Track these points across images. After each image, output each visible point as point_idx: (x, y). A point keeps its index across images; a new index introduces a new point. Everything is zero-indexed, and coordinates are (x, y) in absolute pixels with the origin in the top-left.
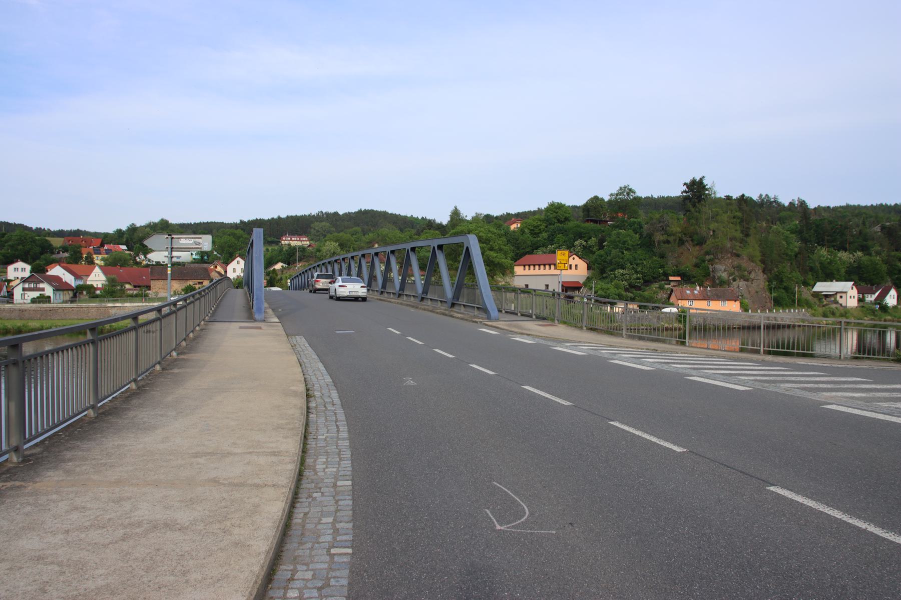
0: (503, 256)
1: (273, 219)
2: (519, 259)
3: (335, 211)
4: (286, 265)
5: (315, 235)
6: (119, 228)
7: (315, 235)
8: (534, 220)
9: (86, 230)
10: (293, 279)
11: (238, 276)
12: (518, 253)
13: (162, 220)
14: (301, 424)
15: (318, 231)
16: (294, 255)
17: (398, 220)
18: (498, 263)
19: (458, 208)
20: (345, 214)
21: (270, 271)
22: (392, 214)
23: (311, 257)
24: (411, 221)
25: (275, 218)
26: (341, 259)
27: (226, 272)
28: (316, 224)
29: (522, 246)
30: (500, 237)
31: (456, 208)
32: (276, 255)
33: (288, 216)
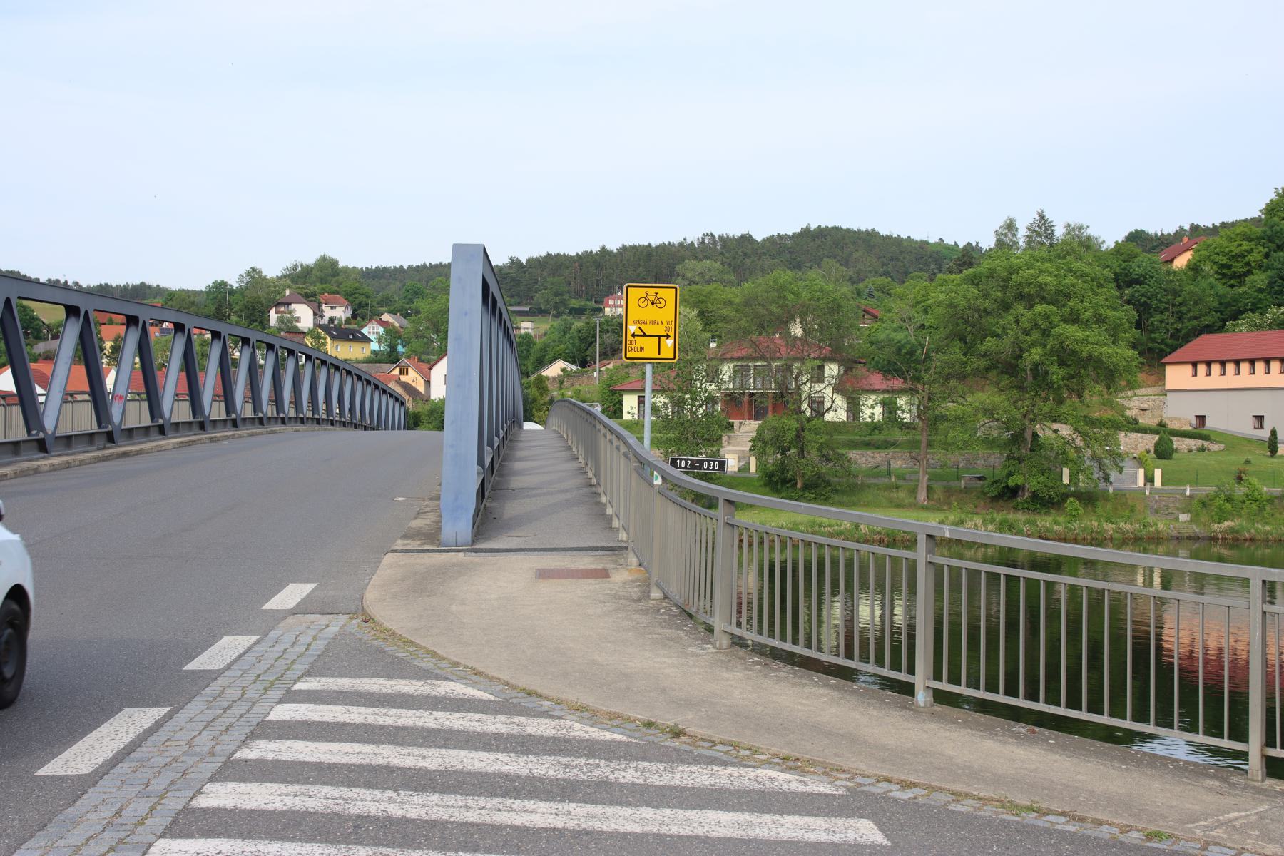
6: (219, 280)
8: (1230, 239)
13: (324, 259)
14: (535, 760)
17: (901, 252)
18: (1090, 358)
19: (1047, 215)
20: (771, 240)
27: (428, 383)
28: (690, 264)
29: (1189, 310)
31: (1042, 217)
32: (554, 341)
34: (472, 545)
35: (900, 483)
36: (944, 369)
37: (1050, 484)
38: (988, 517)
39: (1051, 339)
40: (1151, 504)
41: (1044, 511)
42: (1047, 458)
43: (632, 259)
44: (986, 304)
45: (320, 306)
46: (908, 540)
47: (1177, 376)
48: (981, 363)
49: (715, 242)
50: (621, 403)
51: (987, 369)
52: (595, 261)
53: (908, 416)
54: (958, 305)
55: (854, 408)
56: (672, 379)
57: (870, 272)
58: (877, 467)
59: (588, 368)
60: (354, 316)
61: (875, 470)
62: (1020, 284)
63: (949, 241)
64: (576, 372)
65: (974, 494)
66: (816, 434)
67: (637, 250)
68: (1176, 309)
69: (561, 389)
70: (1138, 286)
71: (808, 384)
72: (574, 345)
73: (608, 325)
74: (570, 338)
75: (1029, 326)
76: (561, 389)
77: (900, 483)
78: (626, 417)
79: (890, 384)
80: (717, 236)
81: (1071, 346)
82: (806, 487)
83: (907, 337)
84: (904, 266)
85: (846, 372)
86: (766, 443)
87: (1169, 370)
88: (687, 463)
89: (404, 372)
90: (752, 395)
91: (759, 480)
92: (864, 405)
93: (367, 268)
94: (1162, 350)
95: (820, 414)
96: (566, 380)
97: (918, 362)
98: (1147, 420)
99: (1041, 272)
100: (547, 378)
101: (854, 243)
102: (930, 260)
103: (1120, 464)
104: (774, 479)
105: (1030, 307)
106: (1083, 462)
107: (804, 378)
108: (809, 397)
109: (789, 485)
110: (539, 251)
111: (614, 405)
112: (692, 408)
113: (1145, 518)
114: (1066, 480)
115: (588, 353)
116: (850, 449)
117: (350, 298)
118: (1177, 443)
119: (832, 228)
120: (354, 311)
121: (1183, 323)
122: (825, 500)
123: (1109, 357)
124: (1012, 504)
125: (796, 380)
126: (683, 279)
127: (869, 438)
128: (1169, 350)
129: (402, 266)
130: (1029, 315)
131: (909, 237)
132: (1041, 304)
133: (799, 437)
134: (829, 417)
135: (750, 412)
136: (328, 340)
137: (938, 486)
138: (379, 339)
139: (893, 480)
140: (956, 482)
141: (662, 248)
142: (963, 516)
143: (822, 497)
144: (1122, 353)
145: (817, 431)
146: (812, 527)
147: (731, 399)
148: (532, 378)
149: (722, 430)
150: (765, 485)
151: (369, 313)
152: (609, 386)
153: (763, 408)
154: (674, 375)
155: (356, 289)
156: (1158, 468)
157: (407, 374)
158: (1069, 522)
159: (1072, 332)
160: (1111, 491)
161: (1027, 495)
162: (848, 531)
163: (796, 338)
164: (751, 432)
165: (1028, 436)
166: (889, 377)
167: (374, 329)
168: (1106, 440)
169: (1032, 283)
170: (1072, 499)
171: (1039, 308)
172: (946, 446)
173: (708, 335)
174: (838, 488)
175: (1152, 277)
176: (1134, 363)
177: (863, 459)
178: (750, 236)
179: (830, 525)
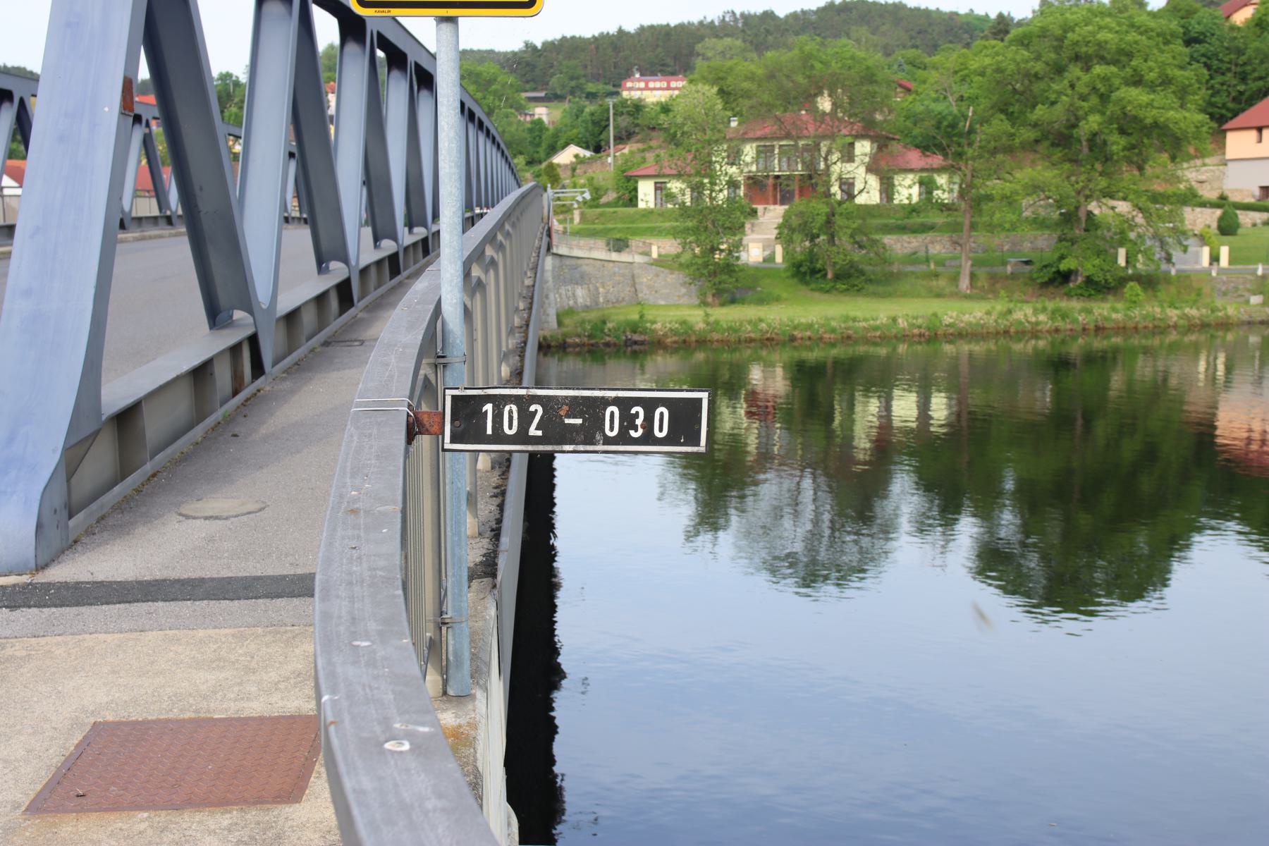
0: (1172, 100)
2: (1243, 110)
3: (767, 8)
6: (224, 72)
9: (582, 36)
12: (1241, 93)
17: (930, 24)
18: (1156, 125)
20: (794, 16)
23: (654, 129)
24: (968, 24)
25: (611, 33)
28: (710, 42)
29: (1254, 70)
30: (1167, 43)
32: (566, 126)
34: (41, 567)
35: (940, 269)
36: (989, 142)
37: (1106, 268)
38: (1039, 306)
39: (1111, 105)
40: (1218, 286)
41: (1101, 296)
42: (1104, 239)
44: (1039, 67)
46: (952, 334)
47: (1239, 143)
48: (1028, 134)
49: (736, 20)
50: (636, 189)
51: (1037, 141)
52: (612, 43)
53: (946, 195)
54: (1006, 70)
55: (888, 189)
56: (689, 161)
57: (898, 46)
58: (915, 253)
59: (602, 154)
61: (913, 257)
62: (1076, 43)
63: (980, 11)
64: (589, 158)
65: (1021, 280)
66: (848, 219)
68: (1239, 69)
69: (573, 176)
70: (1197, 46)
71: (839, 164)
72: (587, 129)
73: (623, 107)
74: (583, 121)
75: (1085, 91)
76: (573, 176)
77: (940, 269)
78: (641, 205)
79: (929, 161)
81: (1134, 112)
82: (838, 277)
83: (949, 107)
84: (933, 38)
85: (880, 148)
86: (792, 230)
87: (1232, 138)
88: (526, 418)
90: (777, 177)
91: (786, 270)
92: (900, 185)
94: (1222, 116)
95: (851, 196)
96: (579, 166)
97: (960, 135)
98: (1209, 193)
99: (1101, 28)
100: (559, 165)
101: (881, 16)
102: (961, 31)
103: (1185, 243)
104: (803, 269)
105: (1087, 69)
106: (1143, 243)
107: (835, 157)
108: (840, 178)
109: (818, 276)
111: (630, 192)
112: (711, 193)
113: (1213, 302)
114: (1122, 261)
115: (602, 137)
116: (884, 234)
118: (1246, 218)
121: (1246, 84)
122: (858, 291)
123: (1176, 123)
124: (1065, 289)
125: (826, 159)
126: (703, 59)
127: (906, 221)
128: (1229, 115)
130: (1086, 78)
131: (938, 9)
132: (1101, 65)
133: (829, 222)
134: (860, 200)
135: (775, 196)
137: (982, 273)
139: (932, 266)
140: (1001, 268)
141: (681, 28)
142: (1011, 305)
143: (856, 288)
144: (1190, 118)
145: (849, 216)
146: (845, 322)
147: (755, 183)
148: (544, 165)
149: (745, 217)
150: (793, 276)
152: (624, 171)
153: (788, 192)
154: (690, 157)
156: (1223, 245)
158: (1128, 309)
159: (1136, 96)
160: (1173, 272)
161: (1080, 280)
162: (885, 325)
163: (824, 113)
164: (777, 218)
165: (1082, 214)
166: (928, 153)
168: (1171, 216)
169: (1089, 42)
170: (1131, 284)
171: (1098, 69)
172: (991, 228)
173: (729, 113)
174: (872, 277)
175: (1213, 35)
176: (1205, 129)
177: (899, 245)
178: (772, 12)
179: (865, 320)
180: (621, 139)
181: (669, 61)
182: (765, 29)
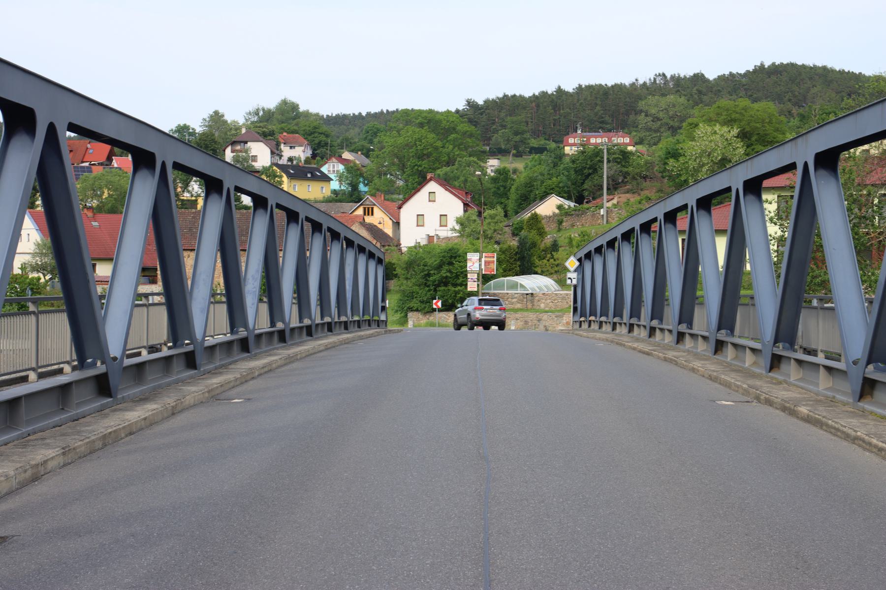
1: (544, 94)
3: (697, 71)
4: (572, 204)
5: (649, 129)
6: (188, 124)
7: (649, 129)
10: (588, 256)
11: (430, 238)
13: (284, 102)
15: (656, 119)
16: (595, 171)
20: (721, 78)
21: (522, 222)
22: (842, 72)
23: (645, 178)
25: (550, 92)
26: (692, 203)
27: (397, 224)
32: (542, 174)
33: (580, 86)
43: (589, 98)
45: (278, 145)
52: (552, 101)
60: (314, 156)
67: (594, 89)
74: (564, 169)
80: (669, 77)
89: (369, 211)
93: (328, 116)
101: (811, 79)
110: (495, 93)
117: (310, 138)
119: (788, 64)
120: (314, 150)
126: (646, 116)
129: (360, 113)
136: (285, 178)
138: (340, 177)
141: (618, 88)
151: (328, 152)
155: (315, 128)
157: (372, 214)
167: (334, 167)
178: (703, 75)
180: (614, 187)
181: (607, 118)
182: (697, 90)
